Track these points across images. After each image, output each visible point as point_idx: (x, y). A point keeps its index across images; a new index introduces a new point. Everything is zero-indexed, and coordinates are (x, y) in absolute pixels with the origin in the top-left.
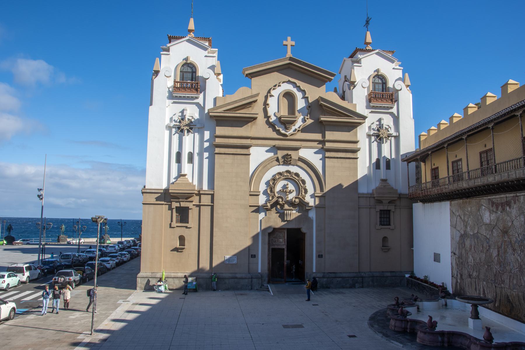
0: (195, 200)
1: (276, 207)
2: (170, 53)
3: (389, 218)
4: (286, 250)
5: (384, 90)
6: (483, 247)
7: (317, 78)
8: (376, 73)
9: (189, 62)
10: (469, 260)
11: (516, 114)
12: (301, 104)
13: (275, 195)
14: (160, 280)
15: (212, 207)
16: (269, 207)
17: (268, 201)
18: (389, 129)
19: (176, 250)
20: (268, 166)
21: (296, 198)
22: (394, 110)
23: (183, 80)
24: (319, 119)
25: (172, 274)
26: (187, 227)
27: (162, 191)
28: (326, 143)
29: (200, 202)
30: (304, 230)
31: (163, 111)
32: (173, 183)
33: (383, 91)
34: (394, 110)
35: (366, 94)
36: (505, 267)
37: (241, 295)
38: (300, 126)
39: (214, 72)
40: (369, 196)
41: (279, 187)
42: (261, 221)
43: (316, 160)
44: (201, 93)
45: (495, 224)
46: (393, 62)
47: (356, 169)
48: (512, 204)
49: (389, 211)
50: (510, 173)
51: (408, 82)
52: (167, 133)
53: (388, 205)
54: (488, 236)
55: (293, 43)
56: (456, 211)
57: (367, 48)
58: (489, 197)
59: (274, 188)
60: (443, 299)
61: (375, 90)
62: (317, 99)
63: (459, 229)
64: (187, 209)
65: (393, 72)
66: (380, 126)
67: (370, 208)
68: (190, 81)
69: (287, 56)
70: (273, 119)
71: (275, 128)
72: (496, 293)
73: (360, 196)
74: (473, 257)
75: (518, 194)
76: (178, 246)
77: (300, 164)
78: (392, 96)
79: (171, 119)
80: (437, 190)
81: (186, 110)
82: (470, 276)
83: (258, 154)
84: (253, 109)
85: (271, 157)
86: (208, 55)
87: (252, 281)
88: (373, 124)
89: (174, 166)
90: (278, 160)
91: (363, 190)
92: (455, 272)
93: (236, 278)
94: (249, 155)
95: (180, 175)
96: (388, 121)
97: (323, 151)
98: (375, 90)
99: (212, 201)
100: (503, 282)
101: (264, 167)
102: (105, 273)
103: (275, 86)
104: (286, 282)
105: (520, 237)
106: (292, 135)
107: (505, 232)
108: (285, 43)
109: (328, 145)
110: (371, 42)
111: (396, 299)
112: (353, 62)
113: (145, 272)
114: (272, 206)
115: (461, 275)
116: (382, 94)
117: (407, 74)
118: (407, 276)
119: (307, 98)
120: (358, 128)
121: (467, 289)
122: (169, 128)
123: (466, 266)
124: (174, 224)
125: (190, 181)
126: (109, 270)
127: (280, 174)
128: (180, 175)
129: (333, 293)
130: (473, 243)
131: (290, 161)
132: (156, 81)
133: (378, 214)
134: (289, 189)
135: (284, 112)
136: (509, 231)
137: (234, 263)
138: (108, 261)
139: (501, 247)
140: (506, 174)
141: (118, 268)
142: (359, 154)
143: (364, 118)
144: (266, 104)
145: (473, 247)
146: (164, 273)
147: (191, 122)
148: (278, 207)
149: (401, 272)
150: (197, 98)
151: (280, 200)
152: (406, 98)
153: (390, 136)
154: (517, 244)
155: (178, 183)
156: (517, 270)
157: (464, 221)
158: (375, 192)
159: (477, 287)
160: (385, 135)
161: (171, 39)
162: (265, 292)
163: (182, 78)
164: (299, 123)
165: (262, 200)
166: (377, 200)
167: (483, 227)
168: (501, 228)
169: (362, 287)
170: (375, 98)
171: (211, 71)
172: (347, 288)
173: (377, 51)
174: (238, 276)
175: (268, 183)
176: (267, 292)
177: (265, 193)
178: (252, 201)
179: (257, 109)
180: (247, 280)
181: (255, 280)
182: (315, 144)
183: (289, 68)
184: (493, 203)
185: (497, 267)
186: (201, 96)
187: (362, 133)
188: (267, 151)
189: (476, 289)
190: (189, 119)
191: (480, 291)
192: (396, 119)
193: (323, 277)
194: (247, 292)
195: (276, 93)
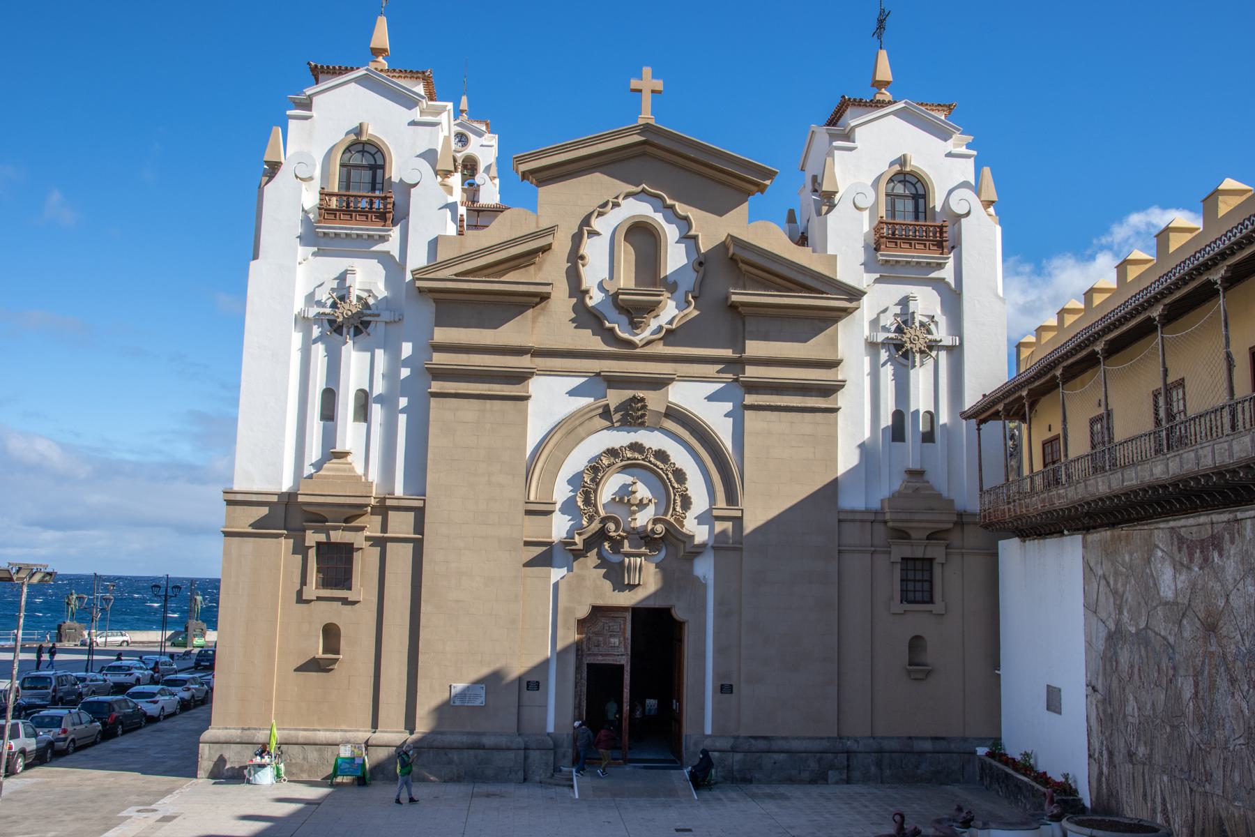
0: (372, 526)
1: (600, 547)
2: (314, 113)
3: (931, 582)
4: (627, 669)
5: (921, 215)
6: (1159, 671)
7: (719, 178)
8: (897, 168)
9: (364, 138)
10: (1129, 709)
11: (1211, 278)
12: (675, 258)
13: (597, 512)
14: (263, 751)
15: (418, 546)
16: (580, 546)
17: (576, 529)
18: (932, 327)
19: (314, 665)
20: (580, 429)
21: (655, 521)
22: (947, 273)
23: (348, 188)
24: (727, 298)
25: (302, 734)
26: (345, 601)
27: (275, 499)
28: (747, 367)
29: (384, 528)
30: (678, 614)
31: (289, 277)
32: (310, 477)
33: (917, 218)
34: (947, 273)
35: (866, 227)
36: (1212, 733)
37: (488, 795)
38: (673, 318)
39: (434, 167)
40: (873, 518)
41: (607, 492)
42: (556, 585)
43: (717, 419)
44: (394, 224)
45: (1186, 602)
46: (945, 135)
47: (833, 440)
48: (1227, 545)
49: (931, 560)
50: (1200, 452)
51: (990, 192)
52: (297, 338)
53: (920, 545)
54: (1171, 639)
55: (659, 85)
56: (1096, 564)
57: (879, 97)
58: (1172, 524)
59: (595, 491)
60: (1055, 825)
61: (894, 216)
62: (724, 243)
63: (1103, 615)
64: (348, 550)
65: (947, 167)
66: (906, 319)
67: (873, 553)
68: (364, 192)
69: (641, 122)
70: (595, 298)
71: (602, 324)
72: (1193, 808)
73: (842, 516)
74: (1136, 698)
75: (1239, 515)
76: (320, 653)
77: (669, 424)
78: (941, 233)
79: (310, 298)
80: (1043, 500)
81: (353, 272)
82: (1131, 755)
83: (551, 399)
84: (540, 269)
85: (589, 406)
86: (418, 118)
87: (526, 758)
88: (885, 311)
89: (315, 426)
90: (606, 413)
91: (853, 501)
92: (1096, 745)
93: (482, 747)
94: (526, 398)
95: (332, 454)
96: (926, 302)
97: (744, 390)
98: (894, 216)
99: (419, 526)
100: (1209, 776)
101: (569, 433)
102: (140, 728)
103: (605, 205)
104: (627, 761)
105: (1247, 644)
106: (649, 343)
107: (1211, 627)
108: (634, 83)
109: (752, 372)
110: (890, 78)
111: (898, 818)
112: (834, 137)
113: (221, 730)
114: (591, 543)
115: (1111, 754)
116: (914, 227)
117: (987, 171)
118: (982, 751)
119: (695, 238)
120: (840, 324)
121: (1124, 795)
122: (303, 322)
123: (1122, 727)
124: (312, 590)
125: (359, 470)
126: (152, 720)
127: (612, 452)
128: (332, 454)
129: (754, 797)
130: (1137, 657)
131: (643, 416)
132: (270, 190)
133: (898, 567)
134: (639, 496)
135: (626, 279)
136: (1221, 623)
137: (477, 703)
138: (154, 695)
139: (1202, 674)
140: (1192, 455)
141: (185, 714)
142: (842, 399)
143: (855, 295)
144: (576, 257)
145: (1136, 671)
146: (275, 730)
147: (366, 306)
148: (606, 545)
149: (965, 739)
150: (383, 239)
151: (611, 526)
152: (983, 237)
153: (933, 346)
154: (1239, 664)
155: (326, 477)
156: (1242, 741)
157: (1115, 593)
158: (886, 505)
159: (1148, 790)
160: (920, 344)
161: (318, 73)
162: (559, 789)
163: (346, 182)
164: (669, 312)
165: (559, 527)
166: (894, 529)
167: (1160, 612)
168: (1202, 615)
169: (848, 781)
170: (893, 238)
171: (425, 166)
172: (801, 782)
173: (901, 105)
174: (488, 741)
175: (575, 481)
176: (566, 789)
177: (569, 507)
178: (532, 529)
179: (552, 271)
180: (511, 755)
181: (535, 755)
182: (711, 370)
183: (644, 154)
184: (1181, 540)
185: (1194, 731)
186: (395, 233)
187: (851, 340)
188: (573, 393)
189: (1145, 795)
190: (359, 298)
191: (1154, 802)
192: (953, 299)
193: (734, 750)
194: (510, 788)
195: (605, 225)
